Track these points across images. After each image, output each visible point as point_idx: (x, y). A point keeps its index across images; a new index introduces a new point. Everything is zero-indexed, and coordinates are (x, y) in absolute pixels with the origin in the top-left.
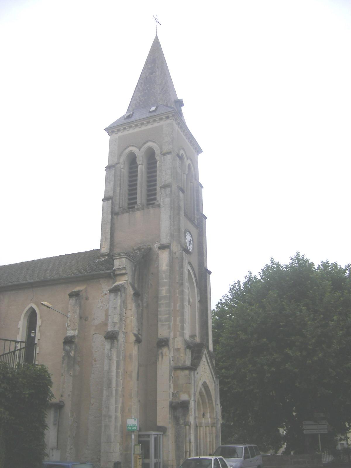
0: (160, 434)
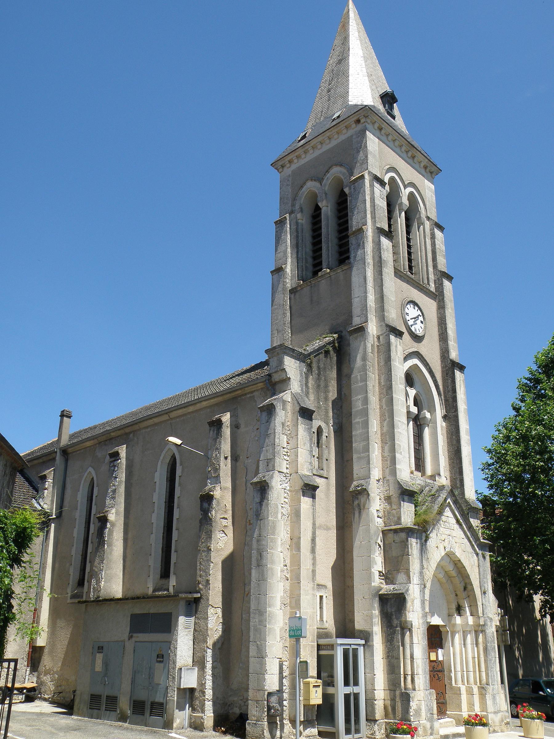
0: (359, 645)
